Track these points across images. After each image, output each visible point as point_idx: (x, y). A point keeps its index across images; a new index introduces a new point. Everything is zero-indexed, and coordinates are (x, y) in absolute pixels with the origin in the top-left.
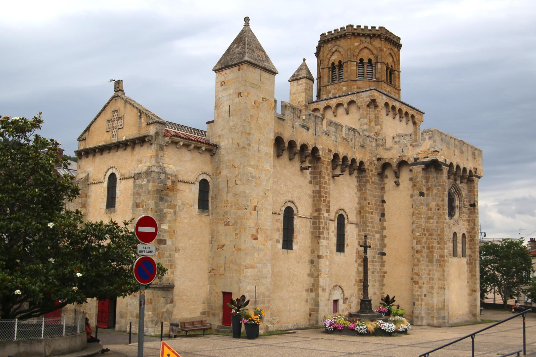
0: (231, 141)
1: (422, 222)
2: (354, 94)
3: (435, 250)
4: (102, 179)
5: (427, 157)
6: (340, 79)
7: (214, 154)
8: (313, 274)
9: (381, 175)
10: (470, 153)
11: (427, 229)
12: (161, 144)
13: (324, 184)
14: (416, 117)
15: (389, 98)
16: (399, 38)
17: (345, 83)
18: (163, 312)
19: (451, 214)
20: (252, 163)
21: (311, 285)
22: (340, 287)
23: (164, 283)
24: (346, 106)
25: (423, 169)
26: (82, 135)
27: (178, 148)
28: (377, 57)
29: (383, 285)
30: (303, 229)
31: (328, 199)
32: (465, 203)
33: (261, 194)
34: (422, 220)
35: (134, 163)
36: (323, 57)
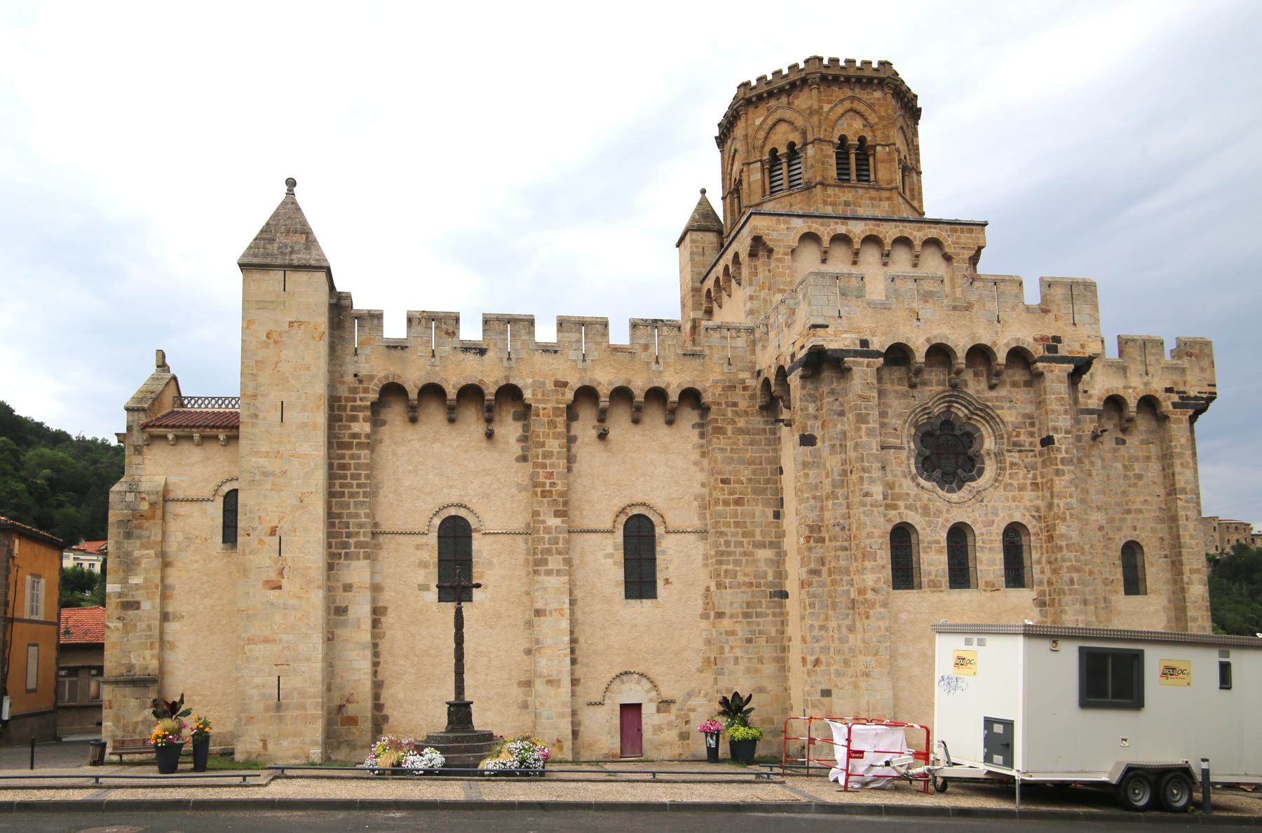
12: (136, 443)
15: (819, 220)
18: (136, 723)
23: (138, 674)
28: (804, 133)
30: (502, 558)
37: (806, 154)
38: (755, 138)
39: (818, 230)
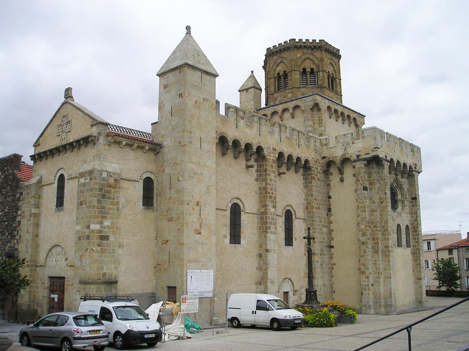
0: (173, 140)
1: (367, 215)
2: (299, 99)
3: (380, 241)
4: (53, 180)
5: (369, 154)
6: (285, 87)
7: (158, 153)
8: (262, 267)
9: (326, 173)
10: (409, 150)
11: (371, 221)
13: (270, 181)
14: (358, 120)
15: (331, 102)
16: (339, 50)
17: (290, 90)
19: (394, 205)
20: (194, 160)
21: (260, 278)
22: (290, 279)
24: (291, 110)
25: (365, 165)
26: (37, 141)
27: (121, 148)
28: (318, 66)
29: (332, 276)
31: (274, 195)
32: (407, 196)
33: (203, 189)
34: (366, 213)
35: (80, 163)
36: (269, 68)
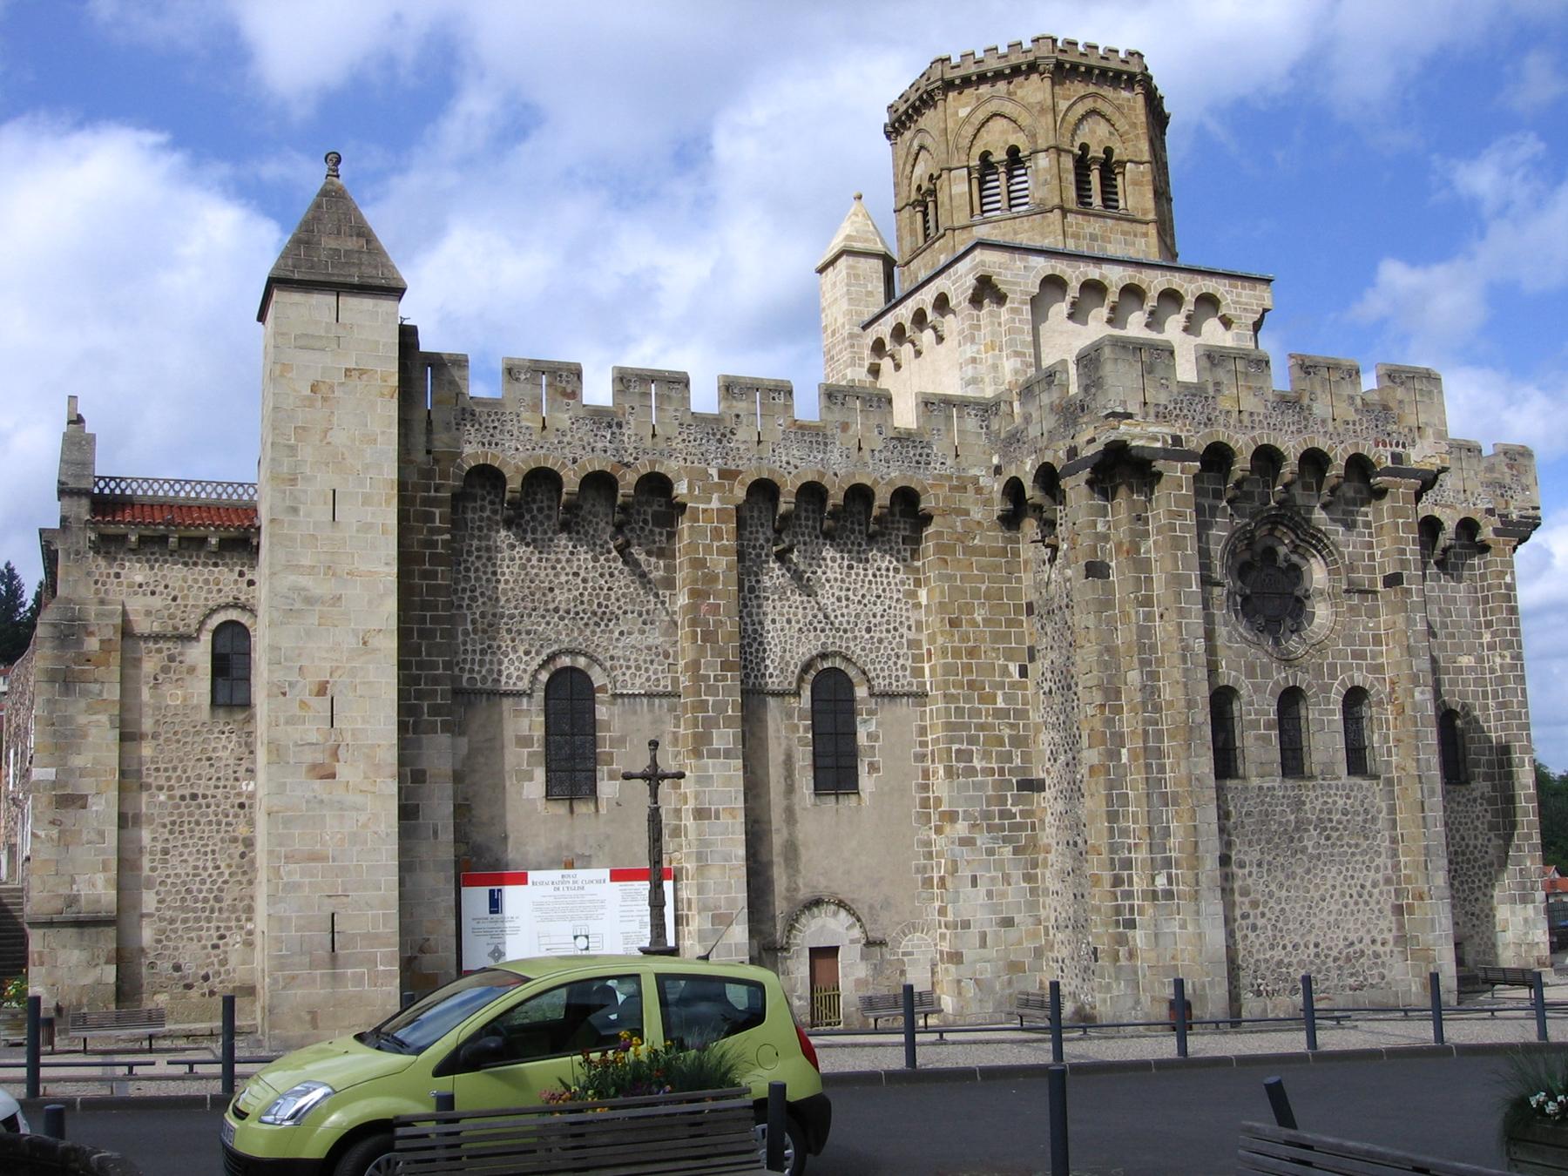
23: (84, 909)
37: (1036, 164)
38: (958, 135)
39: (1064, 272)
